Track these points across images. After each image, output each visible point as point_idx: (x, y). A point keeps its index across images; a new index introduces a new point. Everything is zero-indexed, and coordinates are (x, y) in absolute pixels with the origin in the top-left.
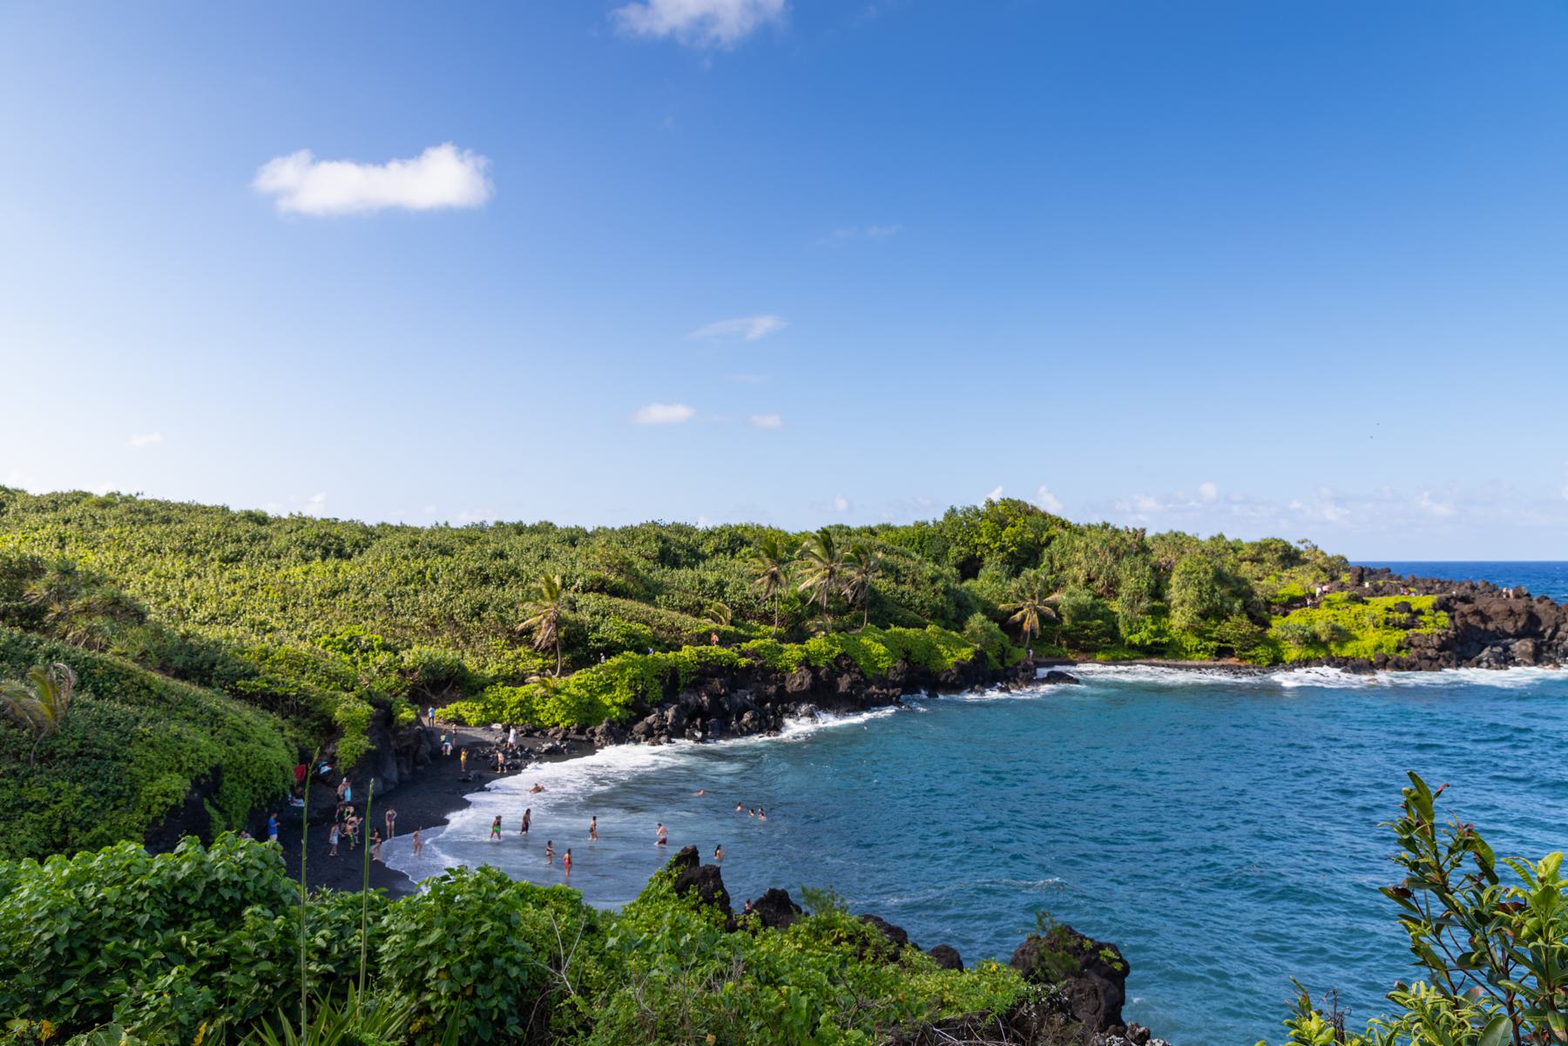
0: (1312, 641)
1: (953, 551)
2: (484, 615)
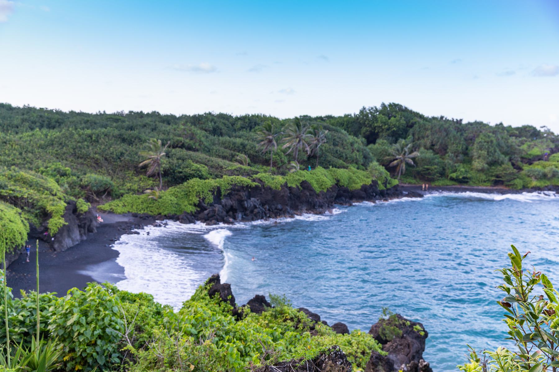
1: (364, 129)
2: (122, 159)
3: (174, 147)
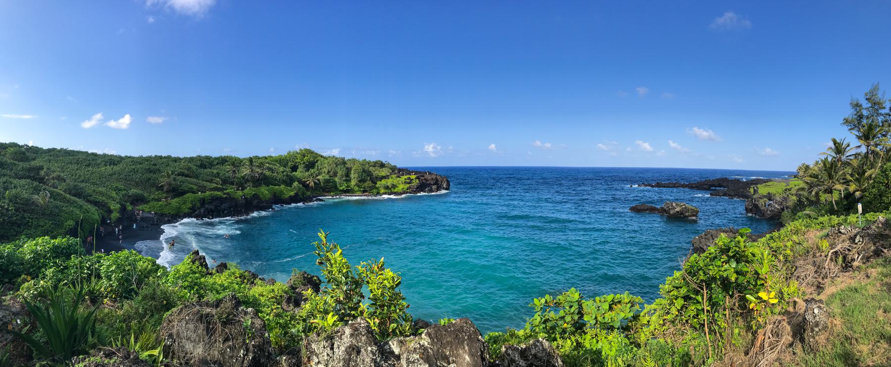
0: (387, 188)
1: (290, 164)
3: (179, 175)
